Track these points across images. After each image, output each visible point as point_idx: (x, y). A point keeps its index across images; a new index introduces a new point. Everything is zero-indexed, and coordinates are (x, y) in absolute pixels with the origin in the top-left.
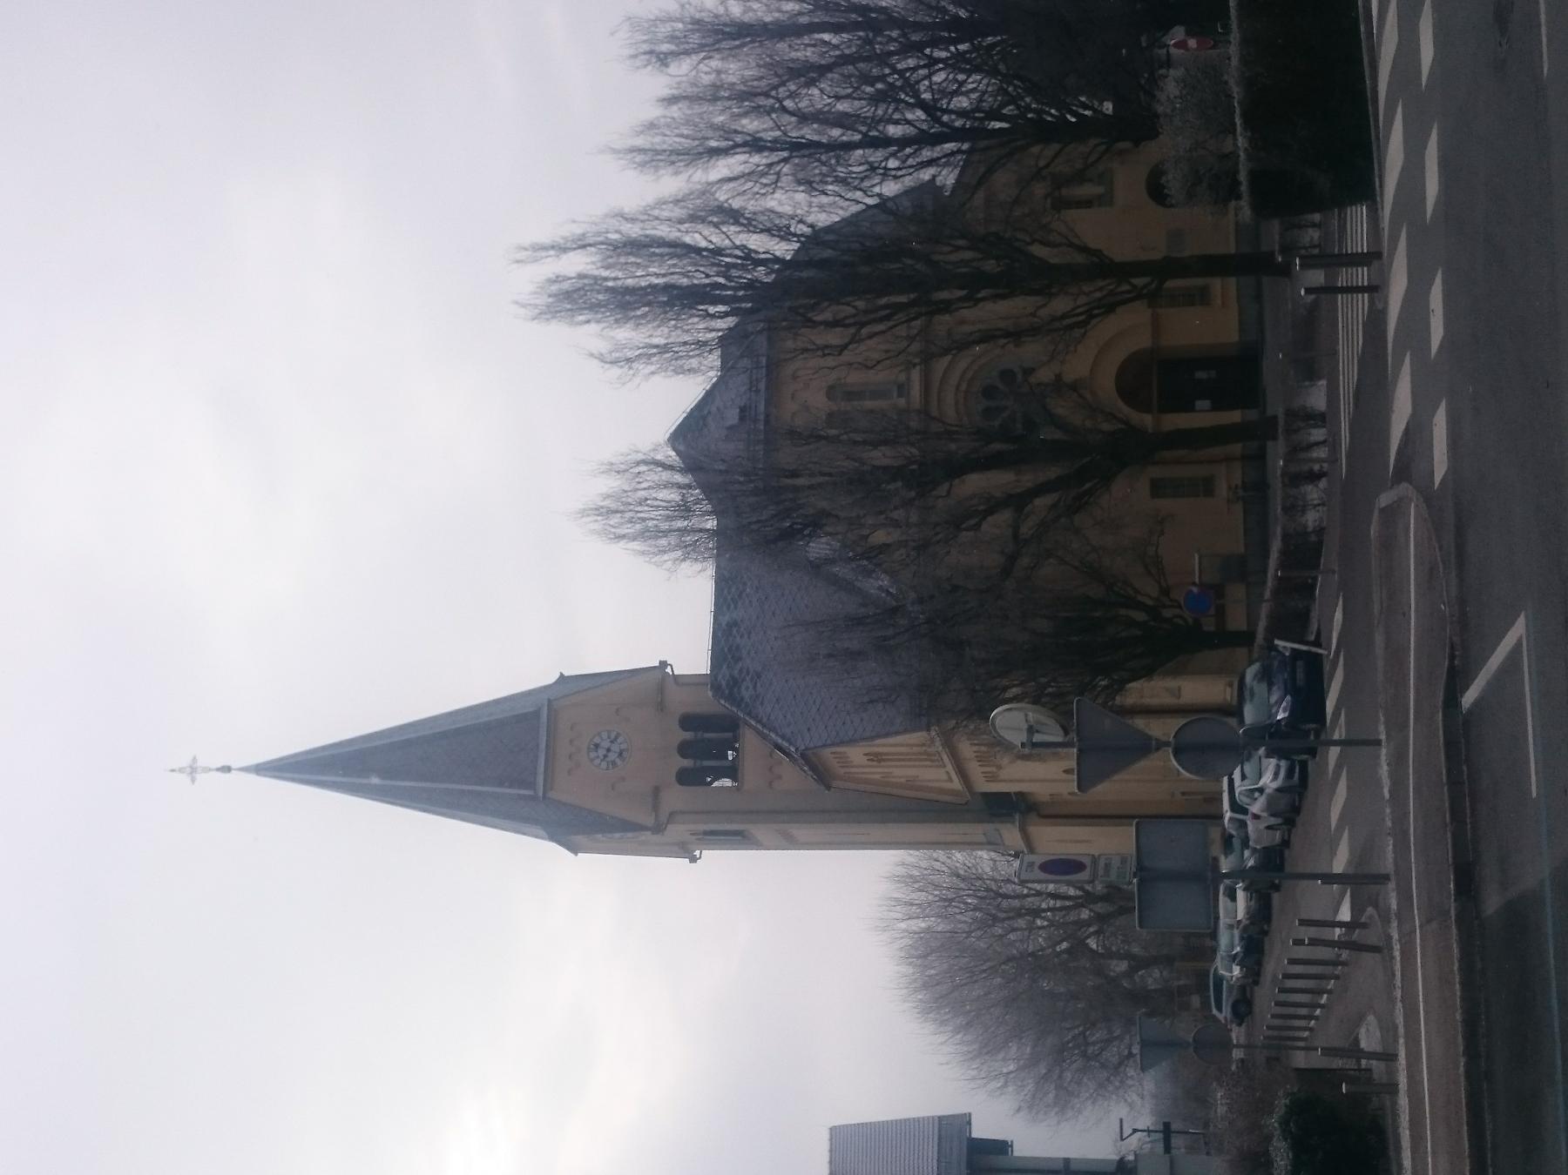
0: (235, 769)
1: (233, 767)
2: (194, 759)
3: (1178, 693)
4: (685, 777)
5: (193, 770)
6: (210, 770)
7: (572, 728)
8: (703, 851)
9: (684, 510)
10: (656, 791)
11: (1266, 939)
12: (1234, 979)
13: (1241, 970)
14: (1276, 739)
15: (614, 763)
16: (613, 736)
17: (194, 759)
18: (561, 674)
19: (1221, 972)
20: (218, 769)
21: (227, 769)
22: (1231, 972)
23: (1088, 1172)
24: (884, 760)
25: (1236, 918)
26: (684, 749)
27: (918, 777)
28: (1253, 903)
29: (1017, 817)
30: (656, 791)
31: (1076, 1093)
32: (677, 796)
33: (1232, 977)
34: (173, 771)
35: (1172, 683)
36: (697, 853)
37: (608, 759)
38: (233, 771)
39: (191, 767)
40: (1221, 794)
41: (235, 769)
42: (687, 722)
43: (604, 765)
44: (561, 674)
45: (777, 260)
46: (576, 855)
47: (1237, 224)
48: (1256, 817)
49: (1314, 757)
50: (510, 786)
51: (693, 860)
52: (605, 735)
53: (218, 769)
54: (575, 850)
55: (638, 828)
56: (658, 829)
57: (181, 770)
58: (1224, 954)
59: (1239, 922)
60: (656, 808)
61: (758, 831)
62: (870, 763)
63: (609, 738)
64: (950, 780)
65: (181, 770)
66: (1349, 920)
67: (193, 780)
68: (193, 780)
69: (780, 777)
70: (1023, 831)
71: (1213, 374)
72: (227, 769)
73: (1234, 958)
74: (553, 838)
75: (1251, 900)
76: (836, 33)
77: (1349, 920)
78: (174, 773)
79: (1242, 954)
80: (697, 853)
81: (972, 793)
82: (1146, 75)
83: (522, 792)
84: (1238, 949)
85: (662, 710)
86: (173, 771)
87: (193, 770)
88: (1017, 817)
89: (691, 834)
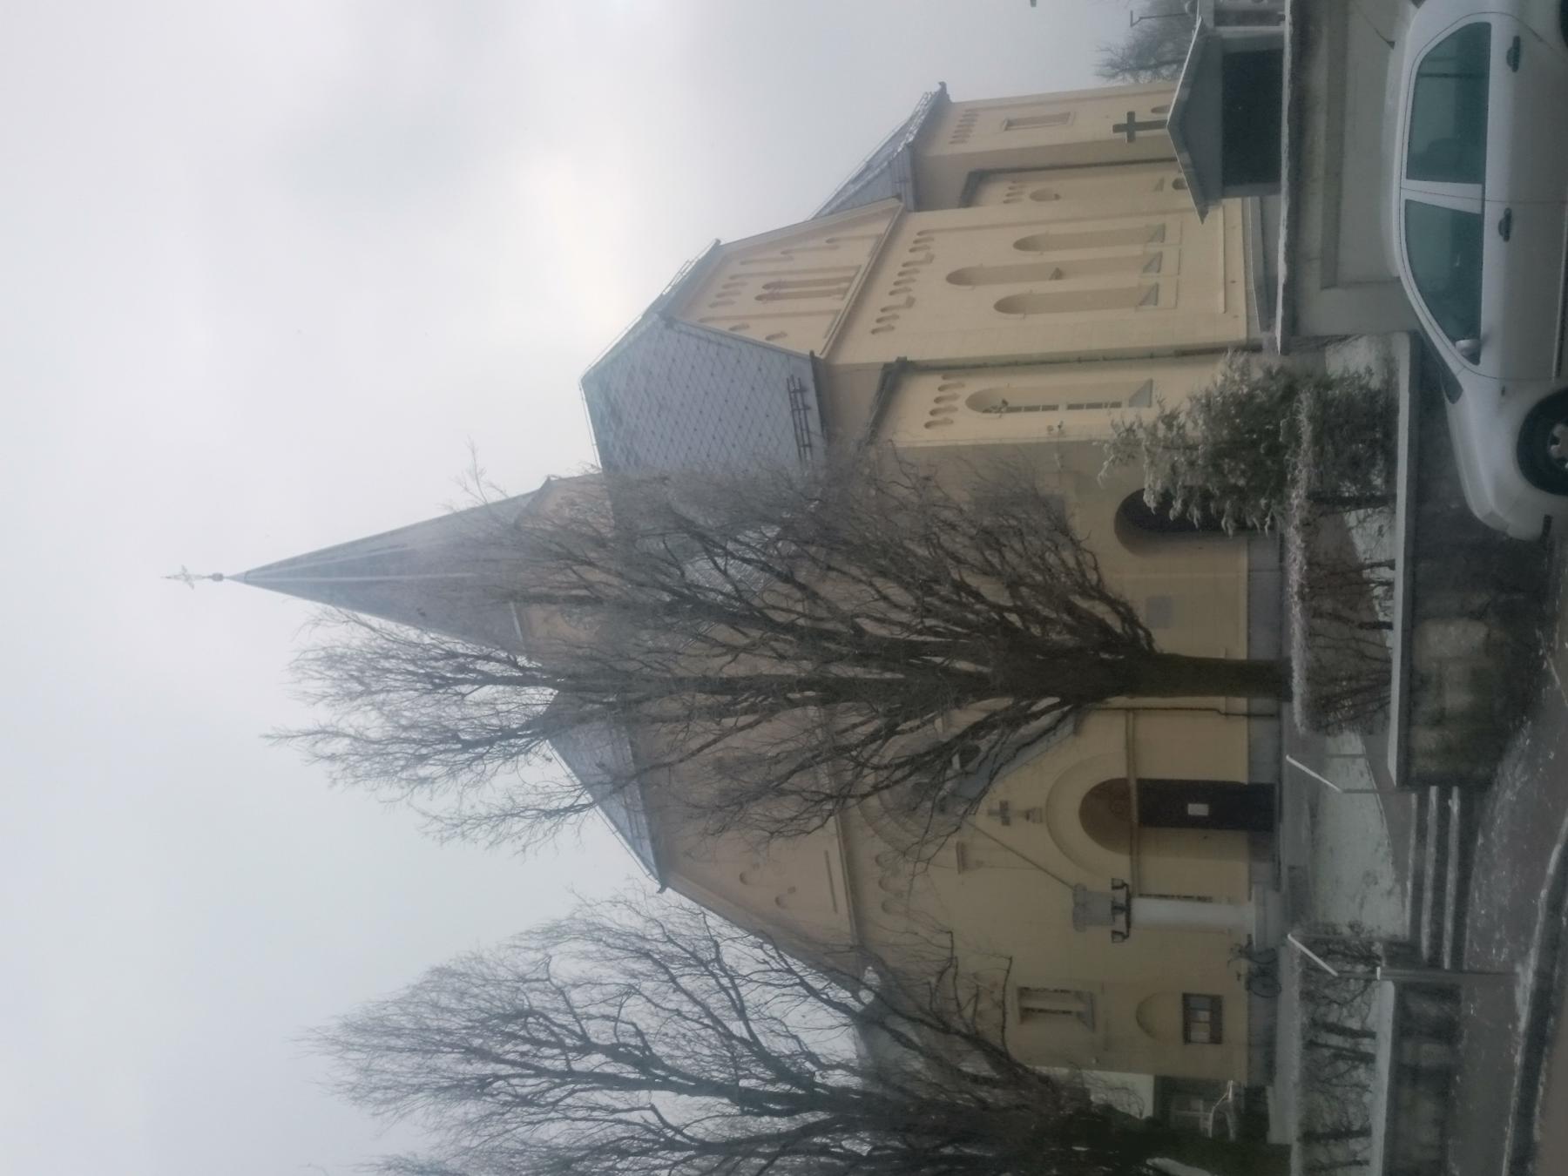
0: (227, 578)
1: (225, 575)
6: (204, 577)
14: (1327, 945)
21: (218, 577)
23: (1566, 40)
31: (1377, 666)
34: (169, 578)
38: (225, 580)
40: (1320, 774)
41: (227, 578)
45: (921, 1098)
47: (1483, 183)
53: (209, 577)
57: (176, 577)
66: (1126, 122)
72: (218, 577)
77: (1126, 122)
82: (1354, 447)
86: (169, 578)
87: (187, 577)
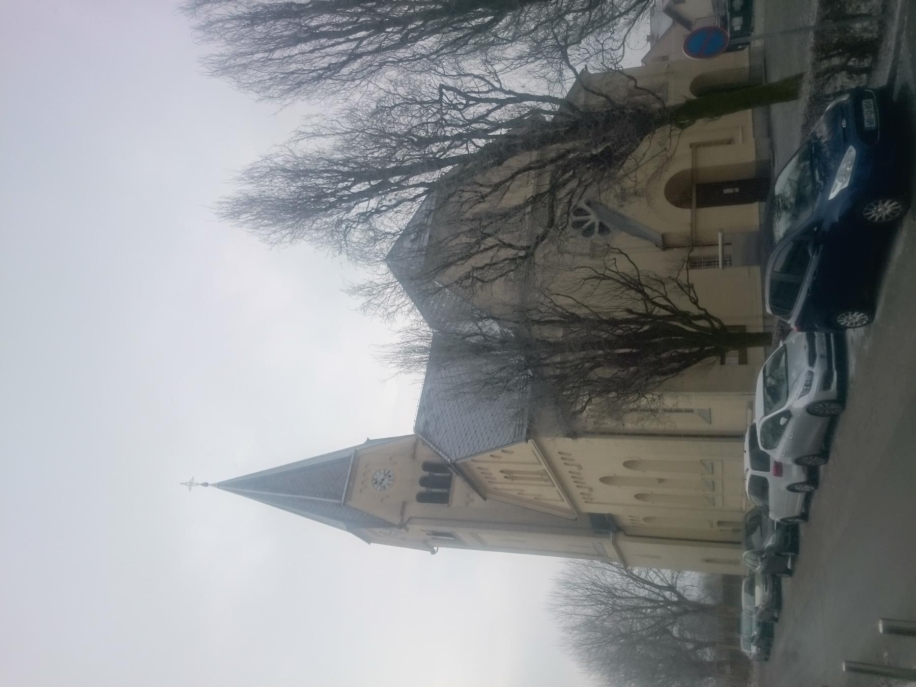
1: (210, 483)
2: (193, 479)
3: (707, 415)
4: (422, 498)
5: (191, 484)
6: (198, 484)
7: (366, 466)
8: (439, 548)
9: (704, 590)
10: (404, 504)
11: (776, 625)
12: (752, 655)
13: (757, 649)
15: (384, 487)
16: (386, 473)
17: (193, 479)
18: (368, 439)
19: (743, 650)
20: (214, 485)
22: (750, 650)
24: (516, 478)
25: (754, 604)
26: (423, 482)
27: (541, 496)
28: (767, 593)
29: (611, 534)
30: (404, 504)
32: (416, 508)
33: (751, 654)
34: (182, 484)
35: (697, 401)
36: (435, 548)
37: (382, 485)
38: (209, 486)
39: (190, 482)
42: (427, 466)
43: (379, 488)
44: (368, 439)
46: (370, 544)
48: (779, 469)
49: (826, 462)
50: (329, 498)
51: (433, 552)
52: (382, 472)
53: (214, 485)
54: (369, 540)
55: (387, 524)
56: (402, 526)
57: (186, 484)
58: (746, 637)
59: (757, 608)
60: (402, 514)
61: (461, 532)
62: (506, 480)
63: (384, 472)
64: (563, 501)
65: (186, 484)
67: (190, 489)
68: (190, 489)
69: (473, 500)
70: (615, 543)
71: (737, 190)
73: (752, 639)
74: (349, 529)
75: (766, 590)
76: (505, 16)
78: (182, 485)
79: (758, 637)
80: (435, 548)
81: (579, 512)
83: (335, 501)
84: (755, 633)
85: (414, 459)
86: (182, 484)
88: (611, 534)
89: (427, 534)
